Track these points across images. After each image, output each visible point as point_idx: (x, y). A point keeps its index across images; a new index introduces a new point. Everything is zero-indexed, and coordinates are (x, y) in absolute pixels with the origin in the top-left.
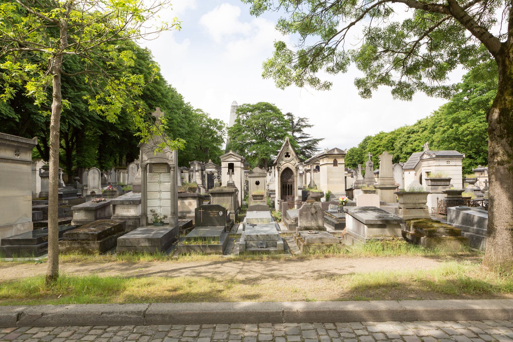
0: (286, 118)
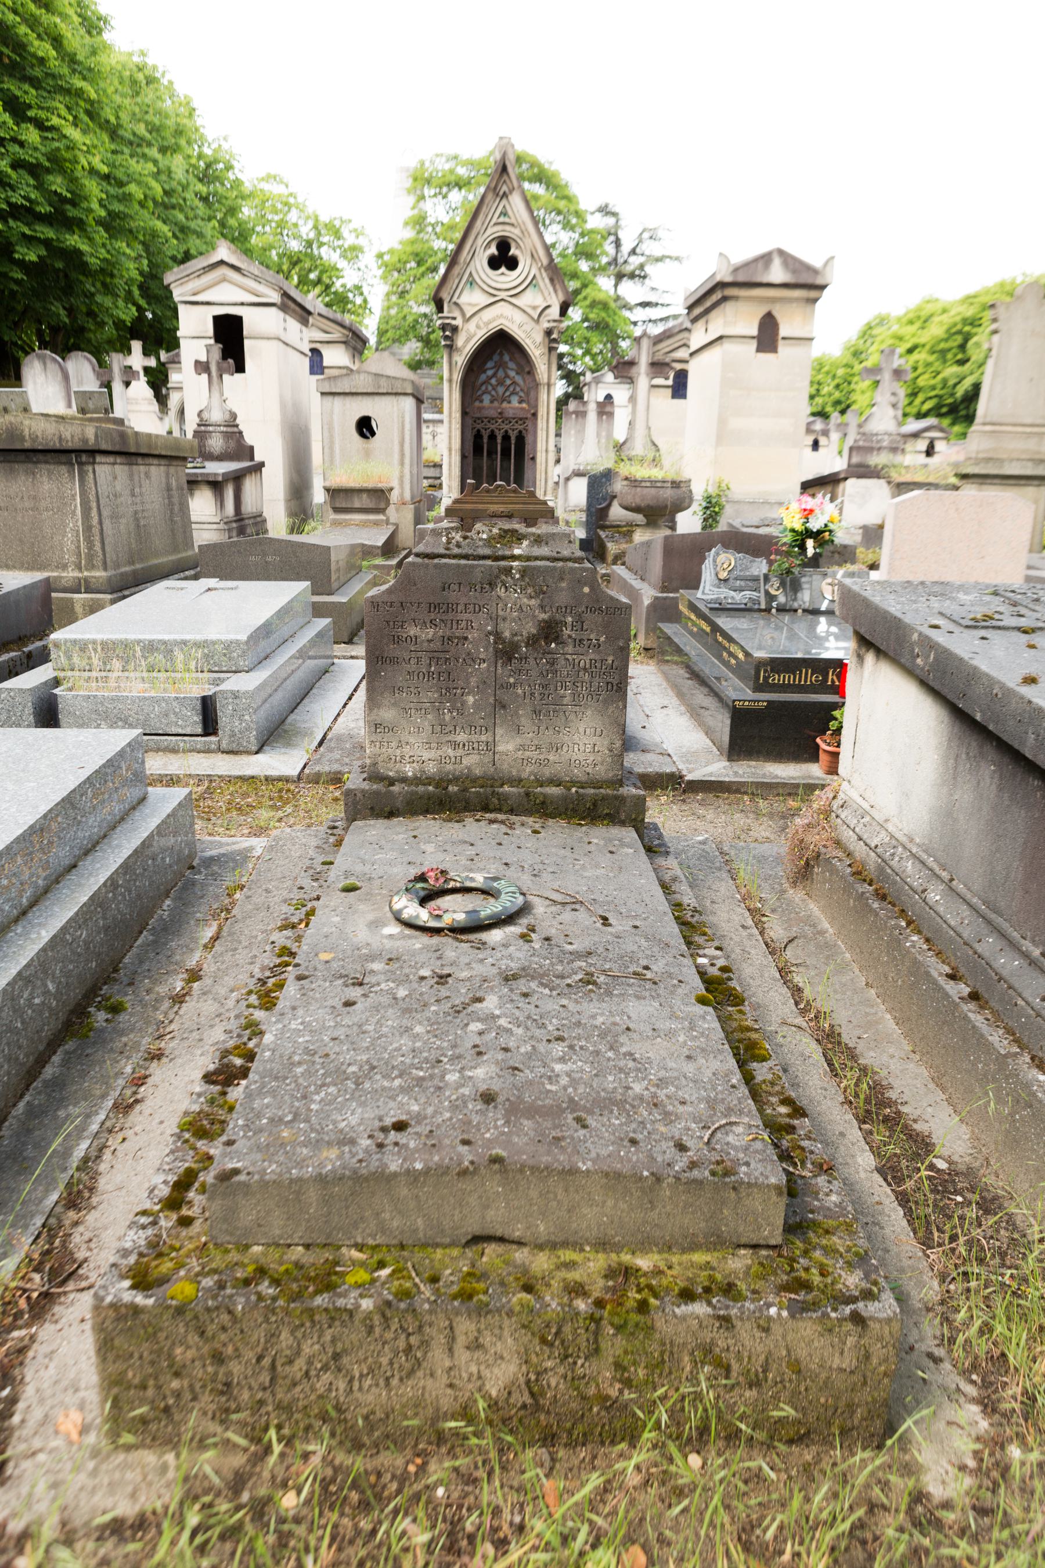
0: (596, 222)
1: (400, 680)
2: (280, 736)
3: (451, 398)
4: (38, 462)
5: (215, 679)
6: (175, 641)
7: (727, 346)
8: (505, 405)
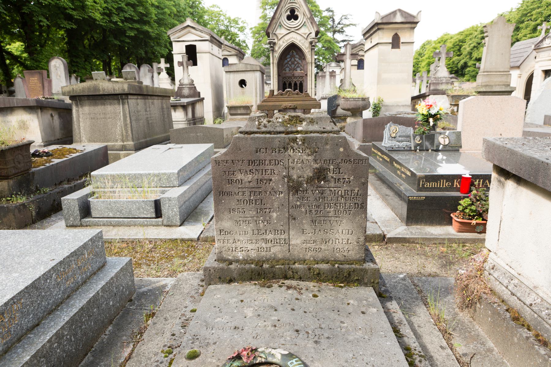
0: (325, 14)
1: (233, 204)
2: (193, 216)
3: (273, 70)
4: (106, 99)
5: (163, 191)
6: (146, 174)
7: (380, 47)
8: (295, 72)
